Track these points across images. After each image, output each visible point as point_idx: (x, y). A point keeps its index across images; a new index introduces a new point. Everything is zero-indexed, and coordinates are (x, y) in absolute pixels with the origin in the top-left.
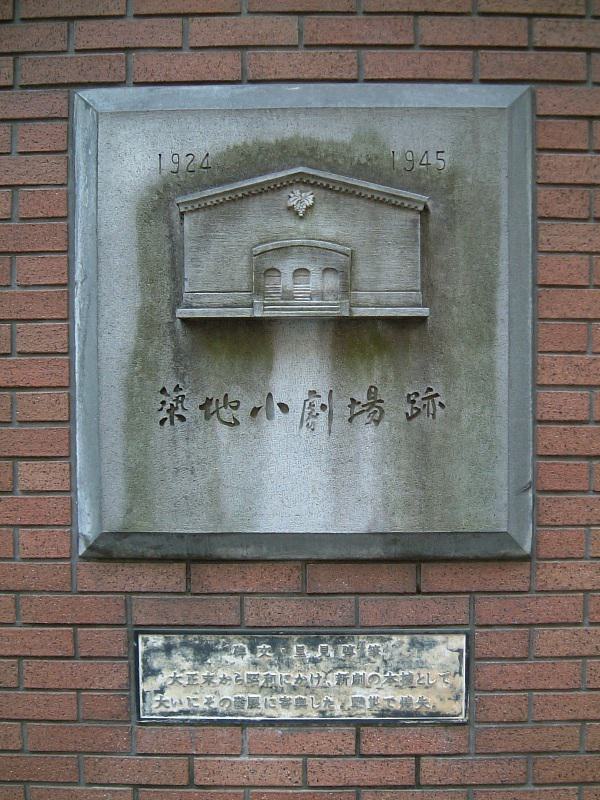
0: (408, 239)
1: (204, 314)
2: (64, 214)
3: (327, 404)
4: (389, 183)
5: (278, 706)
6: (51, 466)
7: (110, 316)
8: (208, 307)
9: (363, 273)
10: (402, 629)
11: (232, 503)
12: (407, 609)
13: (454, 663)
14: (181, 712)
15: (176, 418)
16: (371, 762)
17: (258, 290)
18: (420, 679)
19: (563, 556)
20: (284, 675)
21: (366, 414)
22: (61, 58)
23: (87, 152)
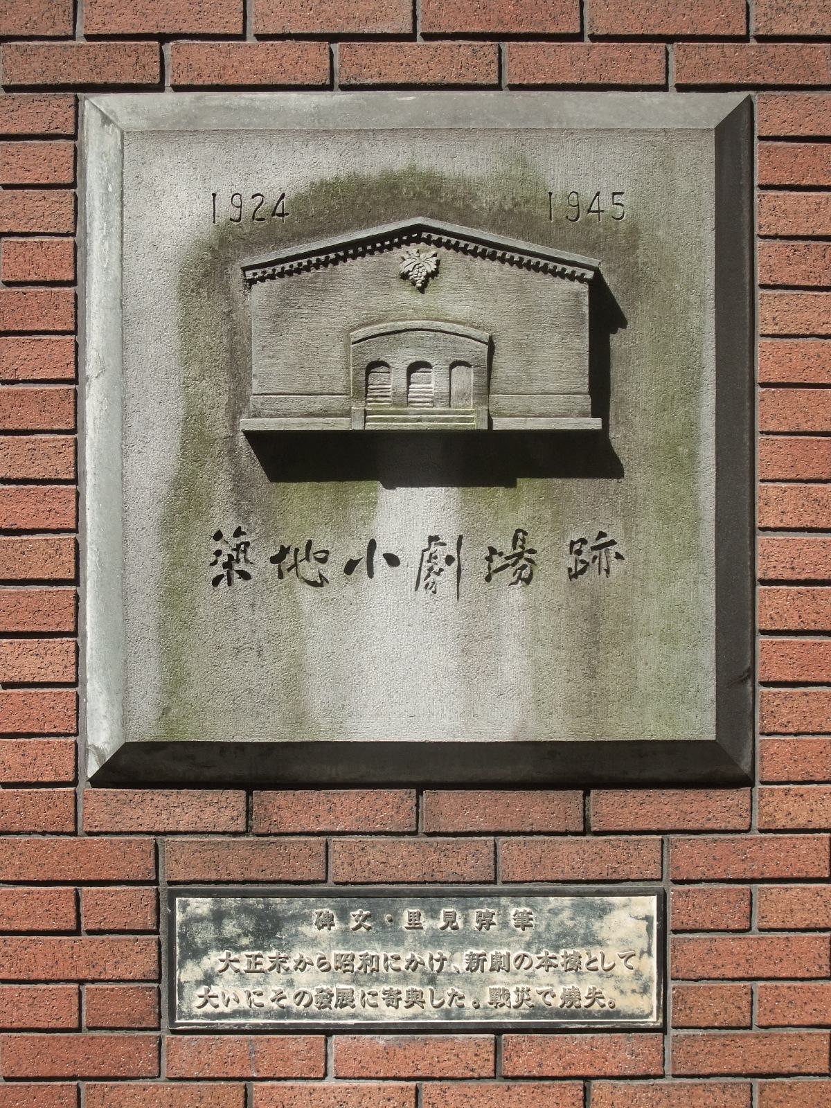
0: (571, 320)
1: (258, 425)
2: (69, 276)
3: (455, 556)
4: (544, 239)
5: (382, 1004)
6: (49, 646)
7: (130, 434)
8: (285, 416)
9: (505, 365)
10: (560, 886)
11: (318, 696)
12: (571, 856)
13: (640, 937)
14: (235, 1014)
15: (236, 575)
16: (520, 1088)
17: (362, 391)
18: (591, 962)
19: (800, 779)
20: (389, 955)
21: (510, 570)
22: (65, 47)
23: (107, 188)
